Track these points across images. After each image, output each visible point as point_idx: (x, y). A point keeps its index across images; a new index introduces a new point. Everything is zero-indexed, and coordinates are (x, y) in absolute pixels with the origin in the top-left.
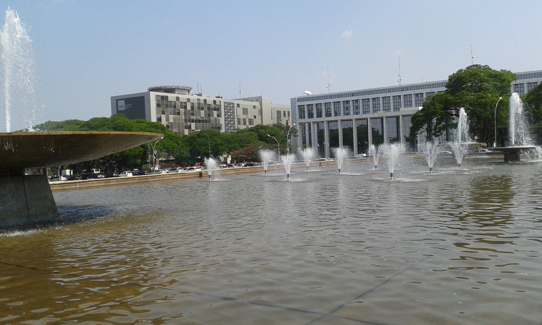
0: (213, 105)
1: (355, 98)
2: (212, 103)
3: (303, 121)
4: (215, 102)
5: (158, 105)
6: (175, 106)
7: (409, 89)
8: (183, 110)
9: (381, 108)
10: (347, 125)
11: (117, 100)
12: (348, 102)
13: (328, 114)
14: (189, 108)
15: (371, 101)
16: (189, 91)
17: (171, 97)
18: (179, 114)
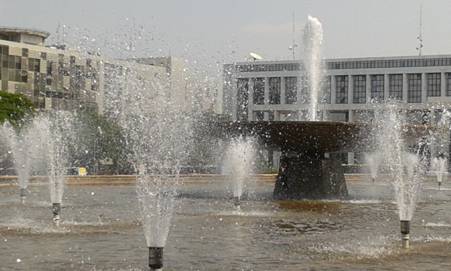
3: (260, 108)
4: (89, 63)
6: (19, 66)
7: (436, 63)
8: (33, 73)
14: (43, 69)
15: (368, 79)
16: (44, 38)
18: (25, 79)
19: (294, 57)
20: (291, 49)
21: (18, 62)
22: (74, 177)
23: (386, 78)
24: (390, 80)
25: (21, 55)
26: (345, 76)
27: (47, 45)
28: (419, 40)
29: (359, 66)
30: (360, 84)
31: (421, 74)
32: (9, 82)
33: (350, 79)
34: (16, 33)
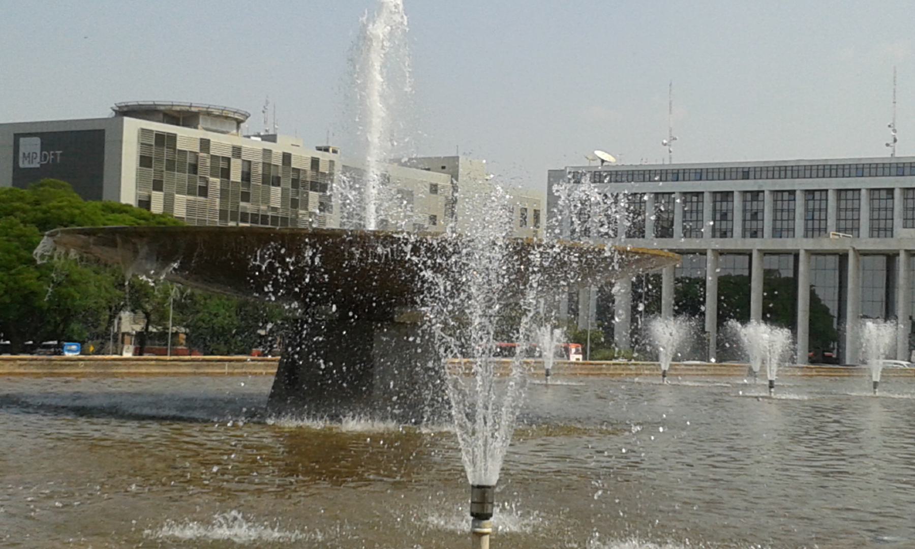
0: (310, 173)
1: (751, 185)
2: (307, 166)
4: (315, 163)
5: (145, 161)
6: (194, 169)
9: (831, 222)
10: (738, 268)
11: (17, 137)
12: (727, 195)
13: (665, 231)
14: (236, 175)
15: (799, 197)
16: (239, 122)
17: (187, 138)
18: (204, 192)
19: (671, 158)
20: (665, 145)
21: (193, 162)
22: (48, 360)
23: (832, 197)
24: (839, 199)
25: (197, 149)
26: (758, 192)
27: (246, 134)
28: (891, 129)
29: (687, 178)
30: (849, 206)
31: (795, 191)
32: (177, 195)
33: (768, 197)
34: (192, 112)
